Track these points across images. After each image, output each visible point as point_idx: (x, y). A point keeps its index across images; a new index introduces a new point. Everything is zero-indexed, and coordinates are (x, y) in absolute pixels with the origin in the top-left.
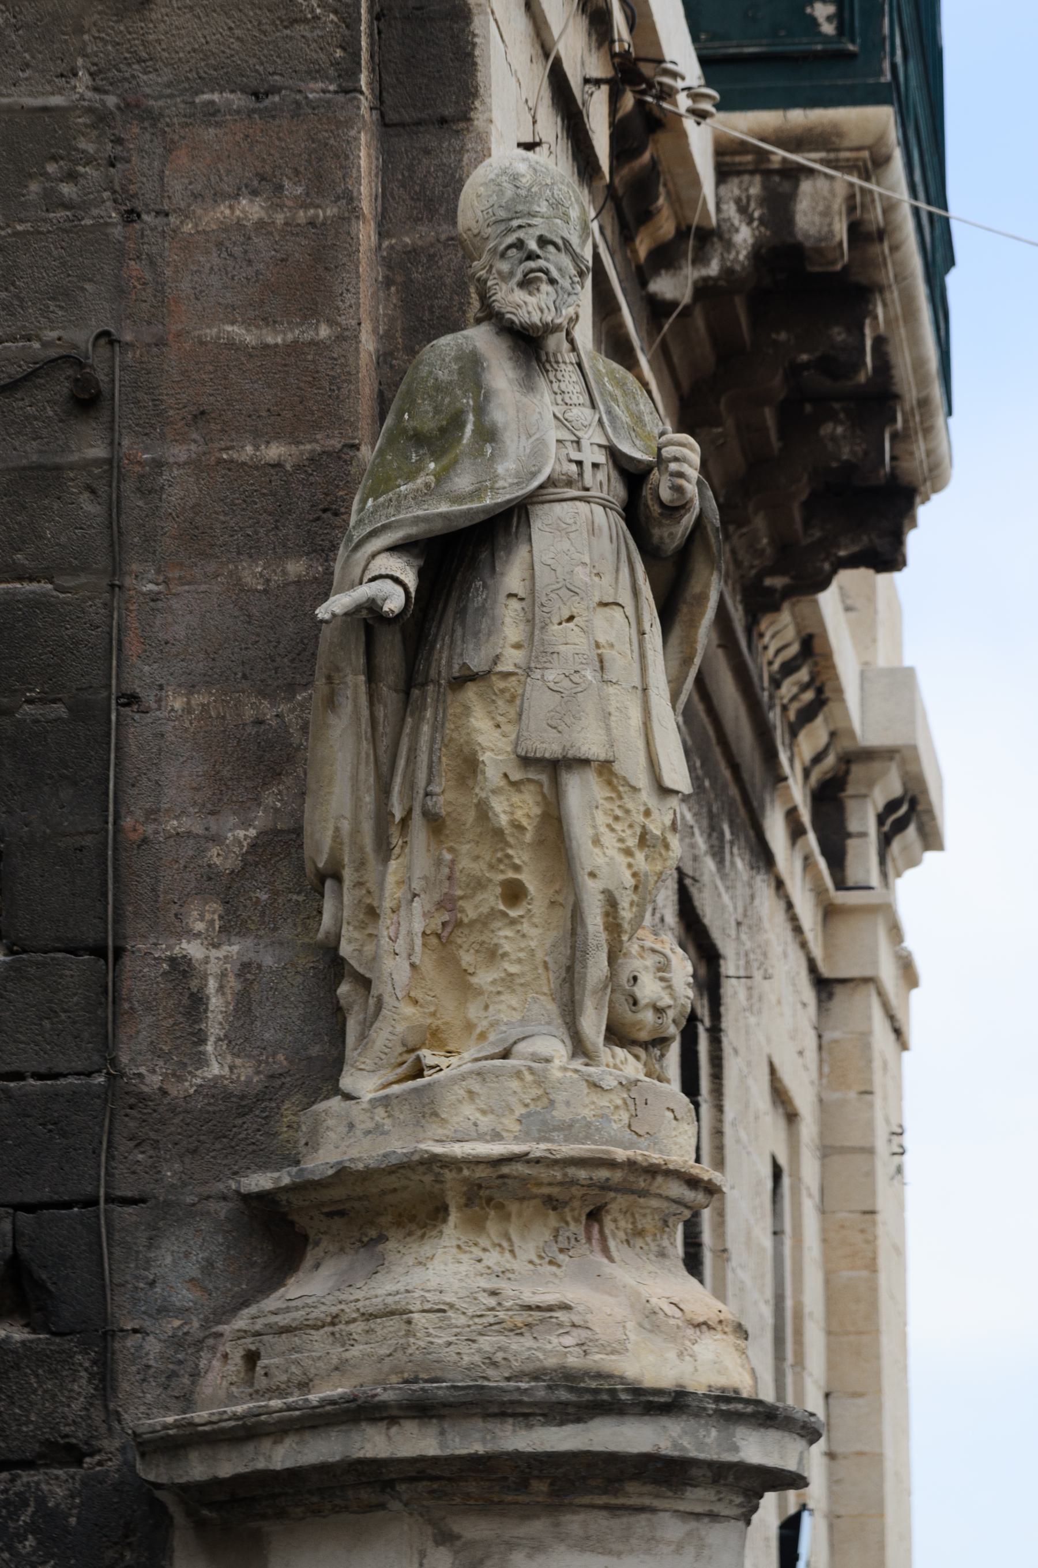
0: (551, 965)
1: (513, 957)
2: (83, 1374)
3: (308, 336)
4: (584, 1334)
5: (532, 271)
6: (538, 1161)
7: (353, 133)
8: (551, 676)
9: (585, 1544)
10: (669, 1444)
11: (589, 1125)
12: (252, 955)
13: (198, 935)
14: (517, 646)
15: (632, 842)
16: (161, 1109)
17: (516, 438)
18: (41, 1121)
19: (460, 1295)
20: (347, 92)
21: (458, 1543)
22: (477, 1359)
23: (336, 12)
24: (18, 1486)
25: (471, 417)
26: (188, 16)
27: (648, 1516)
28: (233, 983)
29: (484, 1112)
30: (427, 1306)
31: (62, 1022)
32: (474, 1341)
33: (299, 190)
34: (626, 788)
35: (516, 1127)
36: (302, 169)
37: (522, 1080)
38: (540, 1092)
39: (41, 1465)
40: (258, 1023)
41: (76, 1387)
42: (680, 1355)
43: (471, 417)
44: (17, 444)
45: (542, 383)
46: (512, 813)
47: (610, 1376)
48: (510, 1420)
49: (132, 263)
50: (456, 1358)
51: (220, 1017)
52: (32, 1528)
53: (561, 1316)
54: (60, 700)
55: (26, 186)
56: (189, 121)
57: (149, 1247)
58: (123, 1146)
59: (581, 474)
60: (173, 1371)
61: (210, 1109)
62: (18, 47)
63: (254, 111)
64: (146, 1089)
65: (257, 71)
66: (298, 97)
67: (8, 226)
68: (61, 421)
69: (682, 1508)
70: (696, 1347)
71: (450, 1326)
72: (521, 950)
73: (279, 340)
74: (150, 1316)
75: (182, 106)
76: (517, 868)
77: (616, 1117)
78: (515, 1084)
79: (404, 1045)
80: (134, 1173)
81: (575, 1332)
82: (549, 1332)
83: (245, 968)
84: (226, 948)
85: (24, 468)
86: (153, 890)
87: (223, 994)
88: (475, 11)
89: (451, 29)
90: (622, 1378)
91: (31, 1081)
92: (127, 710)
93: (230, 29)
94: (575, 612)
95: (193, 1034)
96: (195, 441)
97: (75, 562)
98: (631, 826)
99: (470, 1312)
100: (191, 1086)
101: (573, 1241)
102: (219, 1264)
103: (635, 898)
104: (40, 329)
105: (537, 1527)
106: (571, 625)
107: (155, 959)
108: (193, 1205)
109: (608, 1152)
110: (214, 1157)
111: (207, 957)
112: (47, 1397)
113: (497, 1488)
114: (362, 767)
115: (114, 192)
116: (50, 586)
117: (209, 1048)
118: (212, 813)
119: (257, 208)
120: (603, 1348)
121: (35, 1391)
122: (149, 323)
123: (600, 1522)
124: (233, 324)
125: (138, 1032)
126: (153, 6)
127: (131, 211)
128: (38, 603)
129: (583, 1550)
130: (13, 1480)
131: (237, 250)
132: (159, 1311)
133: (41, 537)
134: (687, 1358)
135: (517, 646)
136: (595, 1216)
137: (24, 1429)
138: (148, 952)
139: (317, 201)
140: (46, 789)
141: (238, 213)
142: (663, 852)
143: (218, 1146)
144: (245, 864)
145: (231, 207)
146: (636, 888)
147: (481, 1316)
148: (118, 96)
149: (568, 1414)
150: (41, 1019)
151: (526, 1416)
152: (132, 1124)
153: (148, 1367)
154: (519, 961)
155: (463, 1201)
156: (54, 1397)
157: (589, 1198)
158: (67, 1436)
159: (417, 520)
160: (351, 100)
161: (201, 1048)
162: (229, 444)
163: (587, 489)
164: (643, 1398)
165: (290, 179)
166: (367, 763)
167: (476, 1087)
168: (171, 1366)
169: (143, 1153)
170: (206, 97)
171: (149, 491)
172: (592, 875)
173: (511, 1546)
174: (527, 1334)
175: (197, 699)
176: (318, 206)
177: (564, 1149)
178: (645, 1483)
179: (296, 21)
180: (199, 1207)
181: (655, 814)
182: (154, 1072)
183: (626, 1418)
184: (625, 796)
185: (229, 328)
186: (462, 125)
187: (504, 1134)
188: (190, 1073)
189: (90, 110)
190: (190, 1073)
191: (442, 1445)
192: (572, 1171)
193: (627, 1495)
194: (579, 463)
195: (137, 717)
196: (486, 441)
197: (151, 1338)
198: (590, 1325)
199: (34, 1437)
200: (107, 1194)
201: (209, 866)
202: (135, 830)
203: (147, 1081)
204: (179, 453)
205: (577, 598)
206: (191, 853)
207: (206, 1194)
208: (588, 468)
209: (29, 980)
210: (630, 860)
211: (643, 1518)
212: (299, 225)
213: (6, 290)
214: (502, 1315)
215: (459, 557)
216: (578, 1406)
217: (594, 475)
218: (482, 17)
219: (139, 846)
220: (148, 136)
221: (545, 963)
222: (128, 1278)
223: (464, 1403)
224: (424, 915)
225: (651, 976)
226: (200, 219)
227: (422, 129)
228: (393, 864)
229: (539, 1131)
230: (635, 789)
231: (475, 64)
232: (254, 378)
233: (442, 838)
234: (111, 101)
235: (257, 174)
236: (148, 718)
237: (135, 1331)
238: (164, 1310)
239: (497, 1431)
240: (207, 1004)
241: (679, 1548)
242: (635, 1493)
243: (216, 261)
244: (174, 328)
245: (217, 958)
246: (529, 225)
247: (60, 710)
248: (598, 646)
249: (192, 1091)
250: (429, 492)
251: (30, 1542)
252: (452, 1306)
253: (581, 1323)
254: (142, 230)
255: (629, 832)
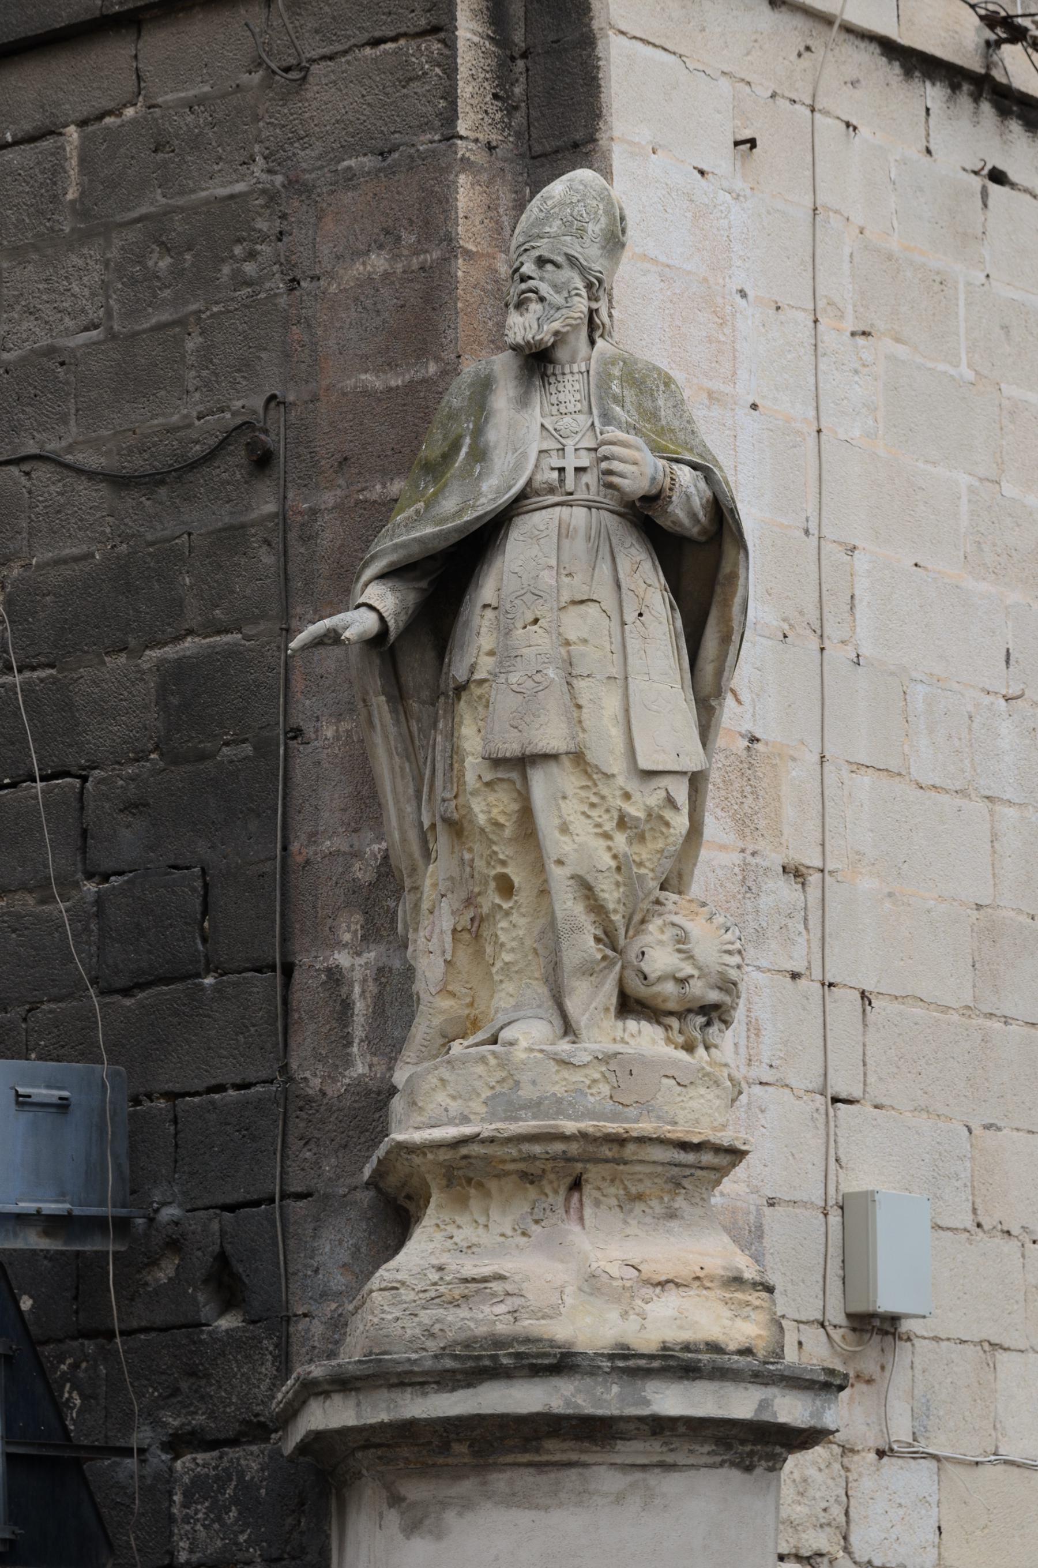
0: (540, 951)
1: (508, 947)
2: (269, 1357)
3: (420, 376)
4: (518, 1301)
5: (523, 292)
6: (492, 1140)
7: (452, 177)
8: (514, 678)
9: (512, 1500)
10: (561, 1403)
11: (559, 1101)
12: (384, 959)
13: (345, 946)
14: (491, 653)
15: (609, 826)
16: (323, 1108)
17: (503, 455)
18: (237, 1128)
19: (413, 1272)
20: (448, 139)
21: (404, 1505)
22: (418, 1331)
23: (439, 65)
24: (225, 1463)
25: (468, 440)
26: (333, 90)
27: (580, 1470)
28: (372, 988)
29: (454, 1098)
30: (384, 1285)
31: (251, 1036)
32: (416, 1315)
33: (413, 238)
34: (600, 776)
35: (483, 1109)
36: (414, 218)
37: (487, 1064)
38: (504, 1074)
39: (245, 1443)
40: (390, 1023)
41: (263, 1370)
42: (624, 1315)
43: (468, 440)
44: (215, 508)
45: (536, 398)
46: (489, 812)
47: (539, 1340)
48: (409, 1389)
49: (294, 327)
50: (400, 1332)
51: (362, 1019)
52: (235, 1500)
53: (496, 1286)
54: (247, 739)
55: (220, 270)
56: (333, 188)
57: (314, 1237)
58: (295, 1144)
59: (562, 481)
60: (332, 1351)
61: (356, 1105)
62: (214, 143)
63: (380, 170)
64: (310, 1092)
65: (382, 132)
66: (412, 151)
67: (207, 309)
68: (246, 482)
69: (619, 1461)
70: (648, 1307)
71: (401, 1302)
72: (514, 939)
73: (400, 382)
74: (315, 1300)
75: (329, 175)
76: (503, 863)
77: (594, 1091)
78: (480, 1069)
79: (444, 1037)
80: (303, 1170)
81: (509, 1301)
82: (483, 1302)
83: (381, 971)
84: (366, 955)
85: (220, 530)
86: (314, 907)
87: (365, 998)
88: (598, 36)
89: (581, 56)
90: (551, 1341)
91: (231, 1092)
92: (293, 744)
93: (363, 96)
94: (538, 614)
95: (343, 1037)
96: (339, 486)
97: (257, 611)
98: (607, 811)
99: (418, 1288)
100: (342, 1086)
101: (548, 1211)
102: (363, 1250)
103: (620, 879)
104: (230, 400)
105: (467, 1486)
106: (535, 628)
107: (316, 970)
108: (345, 1196)
109: (556, 1126)
110: (360, 1150)
111: (353, 965)
112: (244, 1380)
113: (424, 1452)
114: (399, 780)
115: (281, 264)
116: (240, 636)
117: (355, 1049)
118: (355, 831)
119: (382, 261)
120: (535, 1314)
121: (235, 1376)
122: (307, 382)
123: (526, 1478)
124: (366, 372)
125: (304, 1039)
126: (307, 86)
127: (293, 280)
128: (232, 653)
129: (509, 1506)
130: (221, 1458)
131: (369, 303)
132: (321, 1296)
133: (233, 592)
134: (633, 1317)
135: (491, 653)
136: (576, 1185)
137: (228, 1410)
138: (312, 962)
139: (426, 247)
140: (239, 822)
141: (369, 268)
142: (664, 830)
143: (363, 1140)
144: (380, 875)
145: (364, 264)
146: (619, 869)
147: (425, 1291)
148: (284, 174)
149: (459, 1381)
150: (237, 1035)
151: (422, 1384)
152: (302, 1125)
153: (314, 1347)
154: (513, 950)
155: (444, 1182)
156: (248, 1379)
157: (562, 1170)
158: (257, 1415)
159: (396, 547)
160: (450, 146)
161: (349, 1050)
162: (364, 485)
163: (571, 494)
164: (525, 1362)
165: (406, 229)
166: (403, 777)
167: (447, 1075)
168: (330, 1346)
169: (310, 1150)
170: (346, 163)
171: (307, 538)
172: (560, 862)
173: (444, 1505)
174: (464, 1306)
175: (345, 726)
176: (427, 251)
177: (512, 1127)
178: (565, 1440)
179: (411, 79)
180: (349, 1197)
181: (636, 796)
182: (315, 1075)
183: (515, 1381)
184: (599, 783)
185: (363, 377)
186: (590, 146)
187: (472, 1117)
188: (340, 1073)
189: (264, 191)
190: (340, 1073)
191: (358, 1416)
192: (526, 1147)
193: (548, 1452)
194: (561, 470)
195: (301, 748)
196: (477, 461)
197: (316, 1321)
198: (523, 1293)
199: (234, 1417)
200: (282, 1191)
201: (354, 880)
202: (300, 853)
203: (311, 1084)
204: (328, 498)
205: (541, 601)
206: (341, 870)
207: (353, 1185)
208: (570, 474)
209: (228, 999)
210: (610, 843)
211: (573, 1473)
212: (413, 271)
213: (207, 368)
214: (442, 1289)
215: (449, 573)
216: (465, 1372)
217: (577, 479)
218: (604, 40)
219: (304, 867)
220: (305, 208)
221: (535, 949)
222: (300, 1267)
223: (368, 1376)
224: (453, 913)
225: (670, 949)
226: (342, 278)
227: (560, 156)
228: (431, 867)
229: (505, 1111)
230: (609, 776)
231: (599, 86)
232: (382, 420)
233: (464, 840)
234: (279, 179)
235: (383, 229)
236: (309, 748)
237: (305, 1315)
238: (324, 1295)
239: (398, 1400)
240: (353, 1009)
241: (620, 1498)
242: (556, 1450)
243: (354, 314)
244: (324, 383)
245: (360, 965)
246: (533, 248)
247: (248, 749)
248: (568, 643)
249: (342, 1091)
250: (419, 518)
251: (233, 1513)
252: (403, 1283)
253: (516, 1291)
254: (301, 295)
255: (606, 817)
